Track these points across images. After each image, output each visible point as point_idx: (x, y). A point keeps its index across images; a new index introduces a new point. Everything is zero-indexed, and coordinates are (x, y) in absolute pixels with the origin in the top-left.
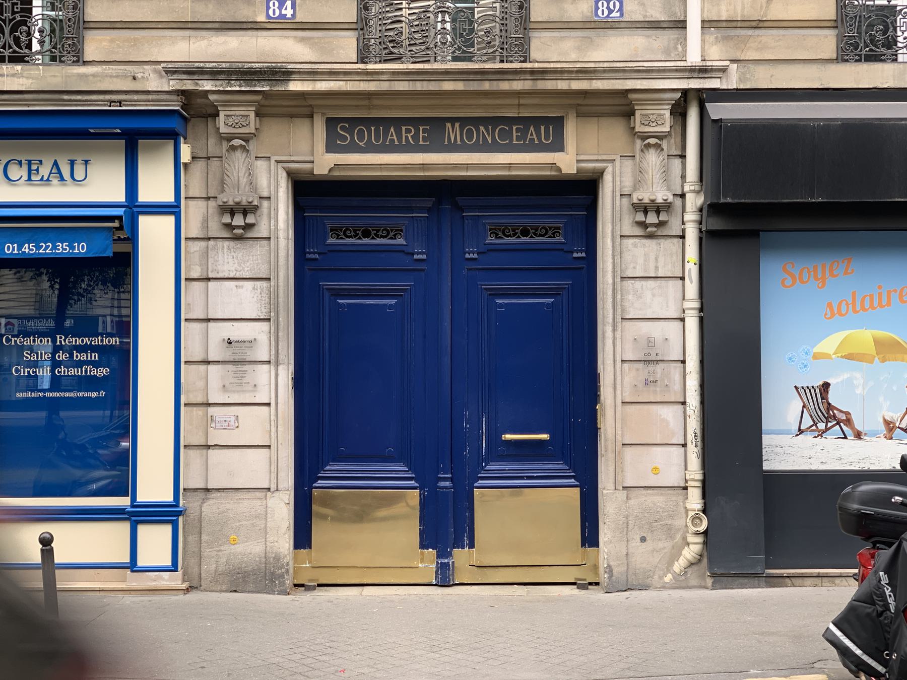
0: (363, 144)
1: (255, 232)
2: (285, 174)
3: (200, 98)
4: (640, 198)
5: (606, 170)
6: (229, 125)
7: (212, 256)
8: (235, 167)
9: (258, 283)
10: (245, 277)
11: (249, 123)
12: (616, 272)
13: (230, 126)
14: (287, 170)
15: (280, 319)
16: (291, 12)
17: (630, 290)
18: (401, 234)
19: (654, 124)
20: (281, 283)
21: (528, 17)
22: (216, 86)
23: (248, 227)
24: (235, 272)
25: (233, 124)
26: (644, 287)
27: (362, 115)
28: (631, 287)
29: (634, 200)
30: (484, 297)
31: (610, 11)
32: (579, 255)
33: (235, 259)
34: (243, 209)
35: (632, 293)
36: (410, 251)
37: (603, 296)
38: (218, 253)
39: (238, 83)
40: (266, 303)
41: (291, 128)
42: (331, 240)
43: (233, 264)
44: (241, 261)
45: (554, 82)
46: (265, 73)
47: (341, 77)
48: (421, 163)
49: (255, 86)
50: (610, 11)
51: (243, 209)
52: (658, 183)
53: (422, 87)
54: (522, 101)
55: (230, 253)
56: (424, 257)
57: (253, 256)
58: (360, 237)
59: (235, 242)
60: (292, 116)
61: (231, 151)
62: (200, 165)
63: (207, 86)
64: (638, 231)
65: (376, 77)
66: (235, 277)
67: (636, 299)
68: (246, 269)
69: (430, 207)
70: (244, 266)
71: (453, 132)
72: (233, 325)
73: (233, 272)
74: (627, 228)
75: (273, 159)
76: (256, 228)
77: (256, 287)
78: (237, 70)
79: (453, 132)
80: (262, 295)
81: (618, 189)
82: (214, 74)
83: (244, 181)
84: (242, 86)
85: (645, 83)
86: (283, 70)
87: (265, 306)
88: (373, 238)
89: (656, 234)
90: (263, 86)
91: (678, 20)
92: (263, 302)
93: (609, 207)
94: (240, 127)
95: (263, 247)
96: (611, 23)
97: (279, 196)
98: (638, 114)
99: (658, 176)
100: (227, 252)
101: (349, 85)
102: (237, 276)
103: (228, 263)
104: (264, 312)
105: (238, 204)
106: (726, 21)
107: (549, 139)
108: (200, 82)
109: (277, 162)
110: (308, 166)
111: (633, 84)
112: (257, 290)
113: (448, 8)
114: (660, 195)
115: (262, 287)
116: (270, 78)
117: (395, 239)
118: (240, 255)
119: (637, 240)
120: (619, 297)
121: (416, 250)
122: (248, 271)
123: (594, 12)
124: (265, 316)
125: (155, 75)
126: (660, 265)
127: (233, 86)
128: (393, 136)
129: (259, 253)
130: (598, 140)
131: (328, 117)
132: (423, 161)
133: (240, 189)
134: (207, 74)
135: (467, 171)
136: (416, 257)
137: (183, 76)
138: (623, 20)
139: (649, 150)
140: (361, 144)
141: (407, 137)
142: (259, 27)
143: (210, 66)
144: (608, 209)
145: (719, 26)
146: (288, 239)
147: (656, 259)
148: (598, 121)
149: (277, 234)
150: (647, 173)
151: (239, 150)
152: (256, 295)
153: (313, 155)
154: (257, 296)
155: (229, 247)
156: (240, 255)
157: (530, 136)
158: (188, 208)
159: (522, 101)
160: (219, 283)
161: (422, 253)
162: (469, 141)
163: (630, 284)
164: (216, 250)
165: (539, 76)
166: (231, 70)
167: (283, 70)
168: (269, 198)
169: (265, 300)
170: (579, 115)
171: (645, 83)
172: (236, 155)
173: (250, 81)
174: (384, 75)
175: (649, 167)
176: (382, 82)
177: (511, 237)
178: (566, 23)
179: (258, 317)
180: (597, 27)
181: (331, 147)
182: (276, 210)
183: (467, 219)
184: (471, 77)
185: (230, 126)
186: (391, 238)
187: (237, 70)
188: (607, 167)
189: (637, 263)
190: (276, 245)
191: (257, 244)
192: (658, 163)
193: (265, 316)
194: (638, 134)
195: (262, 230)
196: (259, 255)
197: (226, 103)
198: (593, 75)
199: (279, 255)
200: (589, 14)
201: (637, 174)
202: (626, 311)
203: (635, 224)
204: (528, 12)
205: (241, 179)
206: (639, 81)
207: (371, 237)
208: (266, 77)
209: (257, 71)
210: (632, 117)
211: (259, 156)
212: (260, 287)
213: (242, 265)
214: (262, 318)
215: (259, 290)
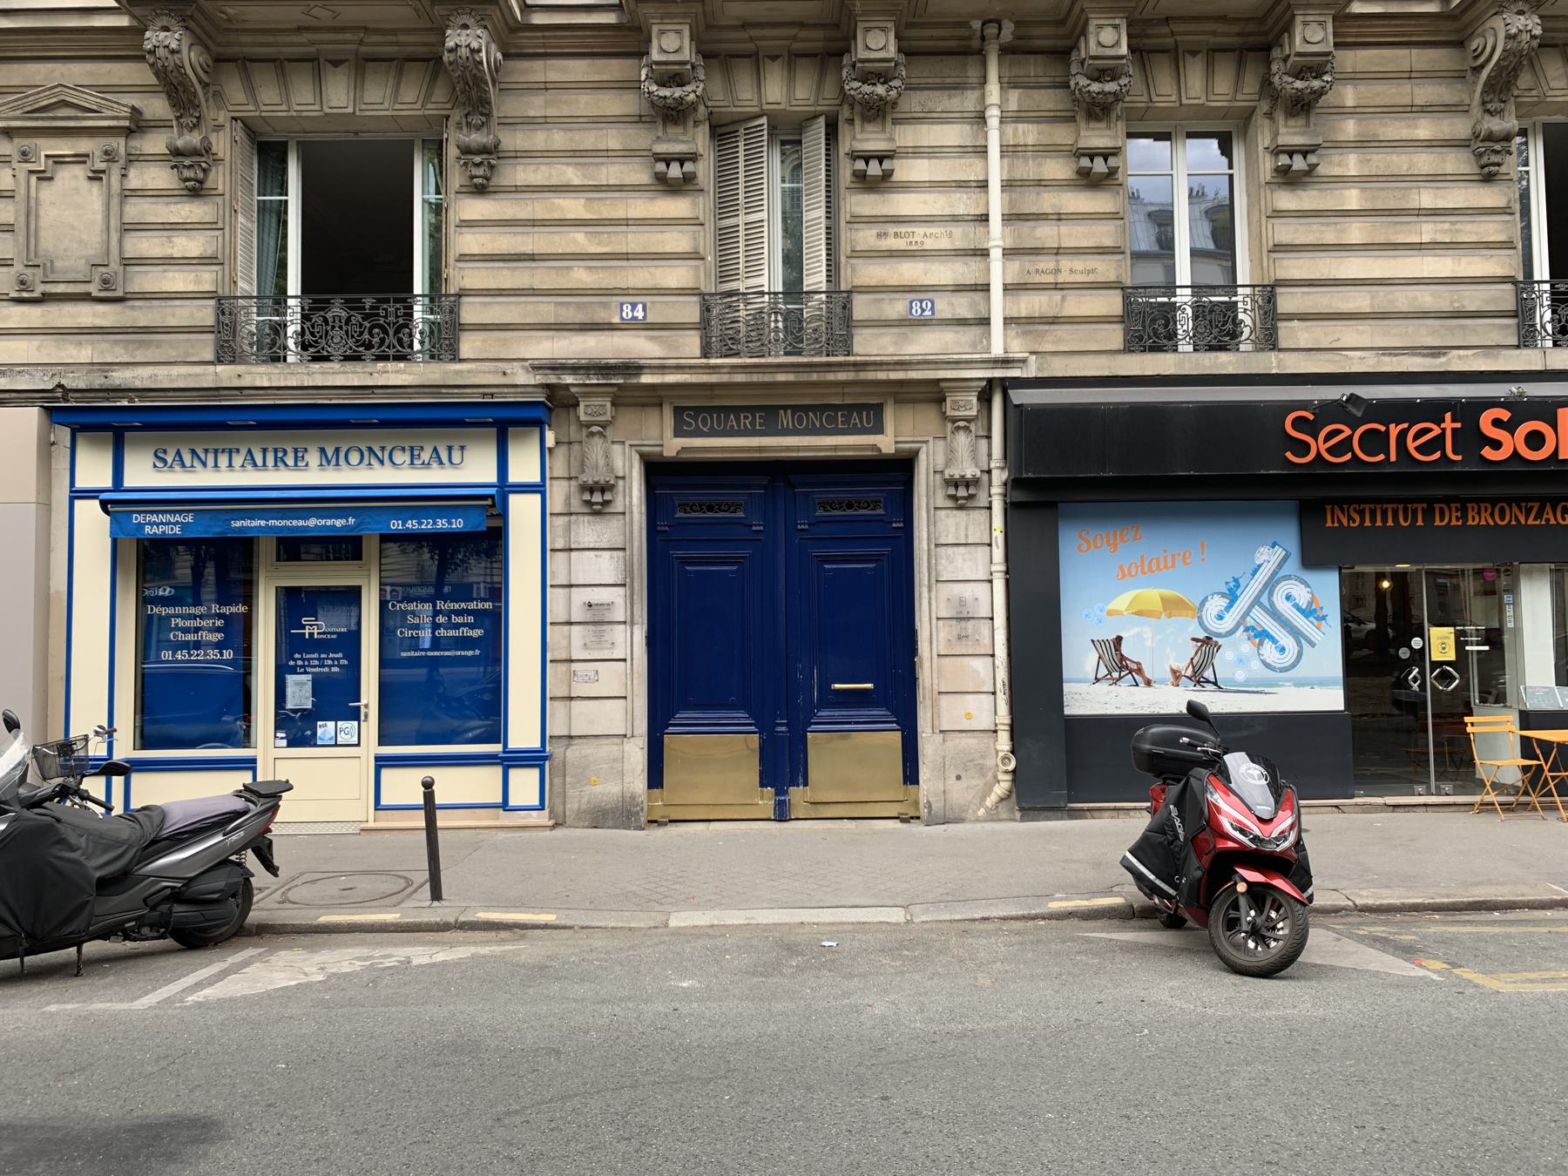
2: (638, 456)
31: (923, 310)
47: (687, 371)
54: (846, 390)
56: (762, 528)
60: (644, 405)
64: (950, 504)
65: (717, 370)
75: (628, 443)
76: (613, 504)
82: (574, 369)
105: (596, 483)
109: (631, 446)
110: (658, 449)
119: (948, 512)
136: (754, 528)
147: (966, 528)
150: (957, 452)
159: (846, 390)
161: (760, 525)
184: (801, 370)
195: (618, 506)
197: (586, 395)
206: (949, 372)
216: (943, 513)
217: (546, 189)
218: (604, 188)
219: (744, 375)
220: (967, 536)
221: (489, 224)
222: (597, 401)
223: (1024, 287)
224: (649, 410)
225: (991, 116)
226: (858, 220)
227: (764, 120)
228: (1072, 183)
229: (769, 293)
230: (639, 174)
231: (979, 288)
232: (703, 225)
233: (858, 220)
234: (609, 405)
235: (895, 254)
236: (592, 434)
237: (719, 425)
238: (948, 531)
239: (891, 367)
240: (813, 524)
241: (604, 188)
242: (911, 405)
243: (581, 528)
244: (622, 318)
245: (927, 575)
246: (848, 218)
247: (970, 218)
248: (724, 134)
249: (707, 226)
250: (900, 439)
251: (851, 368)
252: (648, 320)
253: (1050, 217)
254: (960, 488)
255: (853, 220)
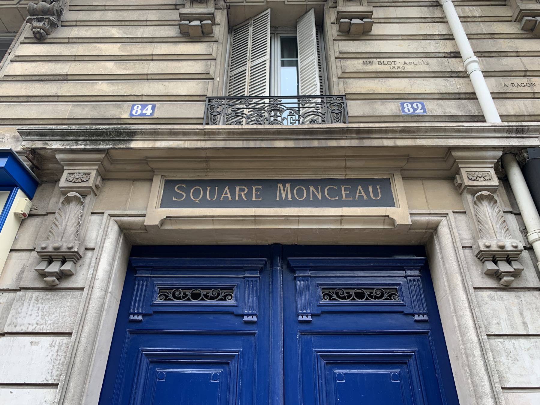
0: (198, 201)
1: (71, 282)
2: (116, 228)
3: (52, 164)
4: (488, 244)
5: (441, 224)
6: (69, 181)
7: (16, 308)
8: (65, 217)
9: (58, 339)
10: (45, 331)
11: (89, 179)
12: (479, 327)
13: (70, 182)
14: (119, 223)
15: (71, 384)
16: (151, 112)
17: (501, 351)
18: (231, 296)
19: (482, 179)
20: (84, 339)
21: (346, 113)
22: (63, 145)
23: (64, 276)
24: (36, 325)
25: (73, 179)
26: (517, 347)
27: (200, 177)
28: (501, 347)
29: (481, 247)
30: (321, 365)
31: (415, 110)
32: (421, 318)
33: (40, 311)
34: (61, 257)
35: (504, 354)
36: (240, 312)
37: (468, 360)
38: (23, 304)
39: (85, 143)
40: (61, 363)
41: (132, 190)
42: (158, 301)
43: (36, 316)
44: (46, 313)
45: (380, 140)
46: (111, 134)
47: (181, 137)
48: (253, 214)
49: (99, 145)
50: (415, 110)
51: (61, 257)
52: (501, 233)
53: (255, 145)
54: (349, 164)
55: (37, 304)
56: (255, 319)
57: (61, 307)
58: (189, 298)
59: (46, 293)
60: (135, 180)
61: (66, 204)
62: (36, 221)
63: (56, 145)
64: (490, 283)
65: (212, 137)
66: (34, 331)
67: (512, 362)
68: (49, 322)
69: (262, 268)
70: (47, 319)
71: (284, 191)
72: (11, 392)
73: (33, 325)
74: (477, 279)
75: (107, 213)
76: (73, 278)
77: (53, 344)
78: (85, 130)
79: (284, 191)
80: (59, 354)
81: (458, 239)
82: (63, 135)
83: (71, 229)
84: (88, 145)
85: (467, 141)
86: (127, 130)
87: (58, 368)
88: (202, 299)
89: (512, 286)
90: (106, 145)
91: (473, 114)
92: (57, 362)
93: (453, 258)
94: (79, 182)
95: (75, 298)
96: (417, 117)
97: (105, 246)
98: (463, 171)
99: (498, 226)
100: (34, 303)
101: (187, 144)
102: (37, 331)
103: (31, 315)
104: (55, 375)
105: (57, 249)
106: (515, 115)
107: (378, 196)
108: (50, 142)
109: (111, 215)
110: (140, 219)
111: (456, 142)
112: (54, 347)
113: (279, 108)
114: (508, 243)
115: (61, 344)
116: (114, 139)
117: (225, 300)
118: (47, 307)
119: (492, 293)
120: (491, 358)
121: (246, 312)
122: (50, 324)
123: (401, 110)
124: (55, 380)
125: (12, 140)
126: (528, 319)
127: (79, 145)
128: (227, 194)
129: (68, 304)
130: (426, 198)
131: (167, 180)
132: (255, 213)
133: (64, 237)
134: (58, 135)
135: (298, 225)
136: (246, 318)
137: (36, 137)
138: (427, 115)
139: (482, 202)
140: (196, 201)
141: (240, 195)
142: (122, 122)
143: (61, 128)
144: (452, 260)
145: (510, 120)
146: (106, 291)
147: (521, 314)
148: (423, 184)
149: (94, 283)
150: (487, 223)
151: (74, 203)
152: (52, 353)
153: (146, 210)
154: (52, 355)
155: (37, 297)
156: (47, 307)
157: (359, 193)
158: (10, 259)
159: (349, 164)
160: (12, 338)
161: (252, 315)
162: (299, 198)
163: (499, 343)
164: (22, 301)
165: (365, 135)
166: (80, 130)
167: (127, 130)
168: (93, 249)
169: (60, 360)
170: (404, 178)
171: (467, 141)
172: (70, 207)
173: (96, 142)
174: (220, 136)
175: (486, 217)
176: (217, 142)
177: (345, 299)
178: (379, 118)
179: (45, 382)
180: (405, 120)
181: (164, 204)
182: (98, 259)
183: (299, 281)
184: (301, 137)
185: (70, 182)
186: (221, 299)
187: (85, 130)
188: (441, 221)
189: (499, 319)
190: (89, 296)
191: (69, 295)
192: (495, 215)
193: (55, 380)
194: (468, 188)
195: (78, 281)
196: (68, 307)
197: (72, 163)
198: (416, 135)
199: (90, 306)
200: (398, 111)
201: (476, 225)
202: (504, 377)
203: (485, 276)
204: (345, 109)
205: (68, 228)
206: (461, 140)
207: (200, 298)
208: (111, 138)
209: (103, 131)
210: (457, 176)
211: (95, 212)
212: (59, 343)
213: (46, 317)
214: (50, 382)
215: (57, 347)
216: (486, 293)
217: (93, 40)
218: (138, 40)
219: (241, 142)
220: (525, 323)
221: (38, 59)
222: (83, 169)
223: (504, 96)
224: (138, 184)
225: (400, 118)
226: (345, 56)
227: (269, 10)
228: (520, 36)
229: (270, 97)
230: (171, 32)
231: (462, 96)
232: (215, 59)
233: (345, 56)
234: (94, 173)
235: (380, 75)
236: (68, 200)
237: (212, 196)
238: (498, 317)
239: (397, 135)
240: (317, 315)
241: (138, 40)
242: (420, 182)
243: (25, 307)
244: (131, 114)
245: (486, 378)
246: (337, 55)
247: (441, 55)
248: (238, 29)
249: (219, 60)
250: (414, 211)
251: (354, 136)
252: (155, 116)
253: (509, 54)
254: (499, 263)
255: (341, 56)
